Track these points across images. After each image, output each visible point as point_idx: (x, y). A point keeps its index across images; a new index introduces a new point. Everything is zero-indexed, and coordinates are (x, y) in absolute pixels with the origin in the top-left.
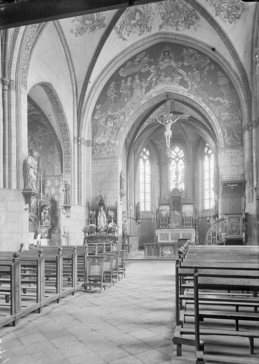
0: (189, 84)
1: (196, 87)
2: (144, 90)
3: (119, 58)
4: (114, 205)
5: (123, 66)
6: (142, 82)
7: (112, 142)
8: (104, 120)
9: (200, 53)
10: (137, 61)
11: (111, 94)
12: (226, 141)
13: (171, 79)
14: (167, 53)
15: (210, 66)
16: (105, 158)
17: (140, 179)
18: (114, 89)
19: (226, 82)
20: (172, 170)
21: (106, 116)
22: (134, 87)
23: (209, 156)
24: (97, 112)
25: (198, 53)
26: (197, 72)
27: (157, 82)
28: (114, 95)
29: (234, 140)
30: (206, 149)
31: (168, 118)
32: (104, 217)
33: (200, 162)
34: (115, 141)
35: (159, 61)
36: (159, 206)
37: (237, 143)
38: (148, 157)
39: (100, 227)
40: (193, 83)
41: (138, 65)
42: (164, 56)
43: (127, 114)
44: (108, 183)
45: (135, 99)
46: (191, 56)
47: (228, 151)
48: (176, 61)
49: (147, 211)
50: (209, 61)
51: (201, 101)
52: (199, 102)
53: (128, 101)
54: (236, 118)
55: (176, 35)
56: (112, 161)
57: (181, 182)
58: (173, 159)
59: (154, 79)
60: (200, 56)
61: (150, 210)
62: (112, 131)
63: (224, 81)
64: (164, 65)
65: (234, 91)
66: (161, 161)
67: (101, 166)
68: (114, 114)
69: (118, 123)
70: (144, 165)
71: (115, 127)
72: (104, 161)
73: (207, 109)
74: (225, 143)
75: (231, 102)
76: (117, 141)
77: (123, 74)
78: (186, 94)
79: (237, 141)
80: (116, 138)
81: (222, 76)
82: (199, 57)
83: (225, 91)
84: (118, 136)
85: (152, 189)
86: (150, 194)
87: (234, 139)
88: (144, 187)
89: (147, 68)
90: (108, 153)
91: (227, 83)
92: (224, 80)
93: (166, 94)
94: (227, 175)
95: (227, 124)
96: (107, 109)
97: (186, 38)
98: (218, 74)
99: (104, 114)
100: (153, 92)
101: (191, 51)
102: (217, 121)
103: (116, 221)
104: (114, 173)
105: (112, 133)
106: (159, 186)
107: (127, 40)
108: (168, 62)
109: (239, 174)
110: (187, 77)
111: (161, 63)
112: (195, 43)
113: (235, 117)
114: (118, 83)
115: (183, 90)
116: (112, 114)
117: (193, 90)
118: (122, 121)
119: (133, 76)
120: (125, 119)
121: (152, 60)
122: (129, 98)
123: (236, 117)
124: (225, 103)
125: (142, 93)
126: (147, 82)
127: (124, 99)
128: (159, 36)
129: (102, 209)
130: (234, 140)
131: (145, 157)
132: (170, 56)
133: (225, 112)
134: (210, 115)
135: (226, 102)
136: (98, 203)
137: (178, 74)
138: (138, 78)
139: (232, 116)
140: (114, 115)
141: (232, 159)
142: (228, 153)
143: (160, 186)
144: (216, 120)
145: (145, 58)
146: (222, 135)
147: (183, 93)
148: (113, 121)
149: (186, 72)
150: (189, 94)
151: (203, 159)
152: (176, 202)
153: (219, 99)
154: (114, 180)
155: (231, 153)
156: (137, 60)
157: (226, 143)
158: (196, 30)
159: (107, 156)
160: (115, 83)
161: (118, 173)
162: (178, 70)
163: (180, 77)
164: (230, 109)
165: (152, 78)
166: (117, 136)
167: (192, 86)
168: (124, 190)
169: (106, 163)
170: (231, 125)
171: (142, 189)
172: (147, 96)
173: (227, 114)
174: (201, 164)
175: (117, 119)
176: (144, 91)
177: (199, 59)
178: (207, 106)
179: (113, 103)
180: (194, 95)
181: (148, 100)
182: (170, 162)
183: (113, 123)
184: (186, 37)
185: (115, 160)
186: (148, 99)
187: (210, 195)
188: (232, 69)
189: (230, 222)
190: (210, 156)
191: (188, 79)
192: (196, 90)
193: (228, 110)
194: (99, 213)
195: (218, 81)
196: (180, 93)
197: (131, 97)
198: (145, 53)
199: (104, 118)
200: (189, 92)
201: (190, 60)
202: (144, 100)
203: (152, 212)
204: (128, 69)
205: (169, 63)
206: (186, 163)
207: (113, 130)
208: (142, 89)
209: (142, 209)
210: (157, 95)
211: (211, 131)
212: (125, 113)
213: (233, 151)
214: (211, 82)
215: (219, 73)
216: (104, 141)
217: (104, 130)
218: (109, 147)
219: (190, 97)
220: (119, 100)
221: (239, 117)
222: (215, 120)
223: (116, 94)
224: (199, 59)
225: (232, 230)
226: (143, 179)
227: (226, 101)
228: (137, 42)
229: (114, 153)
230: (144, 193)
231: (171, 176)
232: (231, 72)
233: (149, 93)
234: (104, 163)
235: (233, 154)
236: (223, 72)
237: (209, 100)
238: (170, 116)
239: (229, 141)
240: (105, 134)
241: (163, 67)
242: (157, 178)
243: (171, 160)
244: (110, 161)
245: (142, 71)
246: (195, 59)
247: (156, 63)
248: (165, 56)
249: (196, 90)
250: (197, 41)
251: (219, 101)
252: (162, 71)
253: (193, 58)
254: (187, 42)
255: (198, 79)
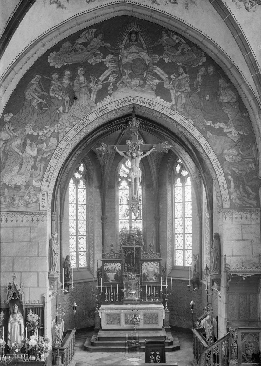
0: (173, 95)
1: (184, 101)
2: (93, 97)
3: (49, 37)
4: (39, 301)
5: (56, 48)
6: (90, 81)
7: (35, 184)
8: (19, 142)
9: (189, 43)
10: (81, 44)
11: (33, 96)
12: (232, 197)
13: (142, 82)
14: (133, 35)
15: (206, 68)
16: (22, 213)
17: (70, 214)
18: (37, 89)
19: (233, 98)
20: (122, 197)
21: (22, 135)
22: (75, 89)
23: (183, 180)
24: (7, 126)
25: (187, 43)
26: (185, 75)
27: (117, 85)
28: (38, 98)
29: (245, 197)
30: (178, 168)
31: (134, 148)
32: (20, 325)
33: (169, 188)
34: (40, 184)
35: (120, 49)
36: (103, 264)
37: (250, 201)
38: (83, 175)
39: (13, 345)
40: (179, 93)
41: (82, 50)
42: (128, 40)
43: (62, 135)
44: (27, 259)
45: (77, 110)
46: (176, 46)
47: (236, 214)
48: (152, 51)
49: (81, 268)
50: (204, 59)
51: (192, 126)
52: (189, 126)
53: (64, 112)
54: (248, 160)
55: (153, 11)
56: (35, 218)
57: (137, 218)
58: (123, 178)
59: (112, 79)
60: (189, 48)
61: (86, 265)
62: (35, 163)
63: (229, 97)
64: (129, 55)
65: (244, 114)
66: (103, 182)
67: (13, 227)
68: (38, 133)
69: (46, 150)
70: (77, 188)
71: (39, 157)
72: (19, 218)
73: (202, 141)
74: (231, 200)
75: (241, 133)
76: (45, 183)
77: (55, 63)
78: (167, 112)
79: (251, 199)
80: (43, 177)
81: (226, 88)
82: (188, 50)
83: (230, 113)
84: (46, 175)
85: (89, 233)
86: (85, 237)
87: (246, 195)
88: (75, 227)
89: (99, 58)
90: (27, 204)
91: (235, 100)
92: (230, 95)
93: (132, 106)
94: (234, 254)
95: (234, 169)
96: (24, 123)
97: (170, 19)
98: (219, 84)
99: (19, 132)
100: (109, 101)
101: (175, 37)
102: (218, 163)
103: (42, 332)
104: (38, 242)
105: (34, 167)
106: (101, 224)
107: (65, 8)
108: (136, 53)
109: (254, 254)
110: (168, 81)
111: (124, 52)
112: (184, 29)
113: (247, 157)
114: (47, 77)
115: (162, 104)
116: (35, 134)
117: (179, 105)
118: (54, 147)
119: (74, 67)
120: (58, 144)
121: (108, 45)
122: (67, 107)
123: (249, 157)
124: (230, 132)
125: (91, 102)
126: (99, 83)
127: (57, 108)
128: (123, 8)
129: (16, 310)
130: (245, 197)
131: (77, 176)
132: (139, 41)
133: (231, 148)
134: (207, 151)
135: (232, 131)
136: (9, 299)
137: (153, 75)
138: (83, 73)
139: (242, 156)
140: (38, 135)
141: (242, 228)
142: (236, 218)
143: (103, 224)
144: (217, 160)
145: (95, 40)
146: (226, 187)
147: (163, 109)
148: (36, 145)
149: (167, 73)
150: (172, 111)
151: (173, 183)
152: (131, 253)
153: (222, 126)
154: (38, 254)
155: (241, 218)
156: (82, 40)
157: (233, 201)
158: (187, 8)
159: (24, 209)
160: (39, 76)
161: (45, 241)
162: (153, 67)
163: (157, 81)
164: (239, 144)
165: (109, 76)
166: (44, 173)
167: (176, 98)
168: (56, 271)
169: (22, 221)
170: (240, 171)
171: (72, 230)
172: (98, 107)
173: (234, 152)
174: (170, 192)
175: (45, 144)
176: (94, 98)
177: (188, 54)
178: (201, 136)
179: (36, 114)
180: (181, 114)
181: (100, 115)
182: (119, 184)
183: (36, 149)
184: (170, 17)
185: (40, 217)
186: (101, 113)
187: (184, 244)
188: (244, 82)
189: (244, 341)
190: (184, 181)
191: (171, 85)
192: (183, 106)
193: (236, 145)
194: (11, 317)
195: (219, 96)
196: (158, 108)
197: (70, 106)
198: (95, 30)
199: (20, 139)
200: (171, 108)
201: (173, 54)
202: (94, 115)
203: (89, 269)
204: (65, 55)
205: (138, 53)
206: (144, 187)
207: (37, 163)
208: (90, 95)
209: (73, 265)
210: (117, 107)
211: (193, 152)
212: (58, 133)
213: (244, 215)
214: (208, 96)
215: (221, 81)
216: (19, 180)
217: (19, 161)
218: (29, 193)
219: (174, 117)
220: (47, 108)
221: (254, 159)
222: (214, 160)
223: (42, 97)
224: (188, 54)
225: (247, 355)
226: (75, 213)
227: (232, 129)
228: (83, 14)
229: (38, 204)
230: (75, 237)
231: (120, 207)
232: (243, 86)
233: (103, 102)
234: (20, 221)
235: (243, 221)
236: (228, 80)
237: (206, 126)
238: (139, 143)
239: (237, 198)
240: (20, 169)
241: (127, 60)
242: (98, 211)
243: (120, 180)
244: (30, 218)
245: (90, 62)
246: (182, 54)
247: (116, 52)
248: (131, 40)
249: (184, 106)
250: (189, 27)
251: (221, 129)
252: (126, 66)
253: (178, 50)
254: (170, 25)
255: (187, 88)
